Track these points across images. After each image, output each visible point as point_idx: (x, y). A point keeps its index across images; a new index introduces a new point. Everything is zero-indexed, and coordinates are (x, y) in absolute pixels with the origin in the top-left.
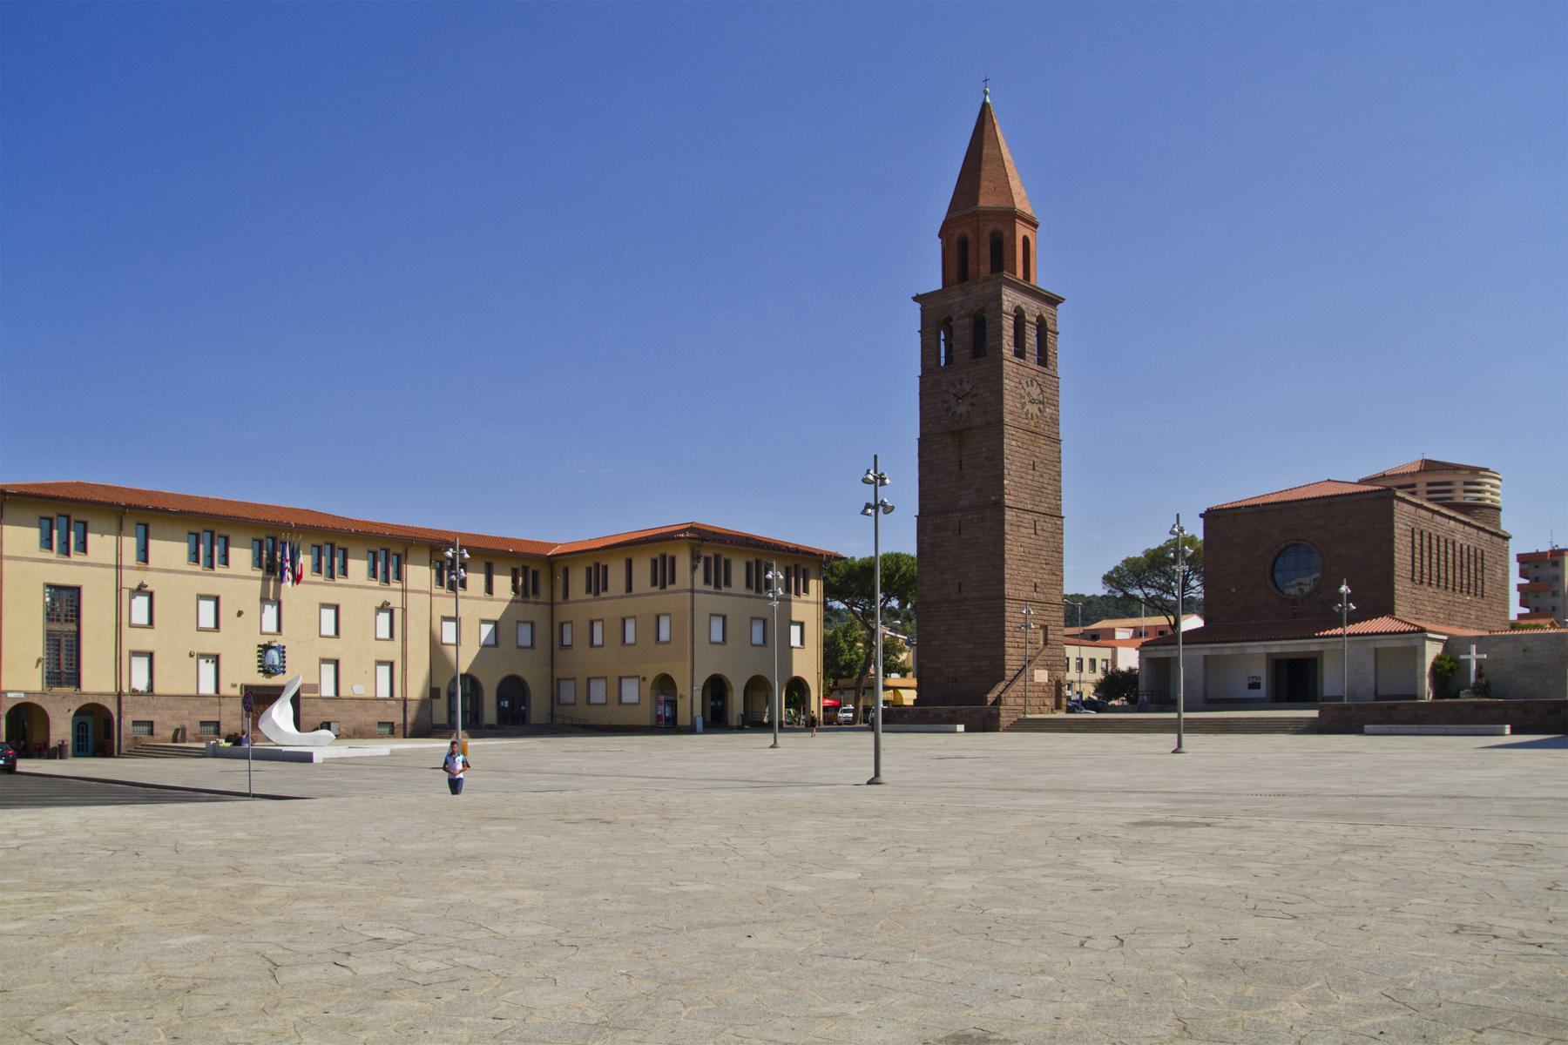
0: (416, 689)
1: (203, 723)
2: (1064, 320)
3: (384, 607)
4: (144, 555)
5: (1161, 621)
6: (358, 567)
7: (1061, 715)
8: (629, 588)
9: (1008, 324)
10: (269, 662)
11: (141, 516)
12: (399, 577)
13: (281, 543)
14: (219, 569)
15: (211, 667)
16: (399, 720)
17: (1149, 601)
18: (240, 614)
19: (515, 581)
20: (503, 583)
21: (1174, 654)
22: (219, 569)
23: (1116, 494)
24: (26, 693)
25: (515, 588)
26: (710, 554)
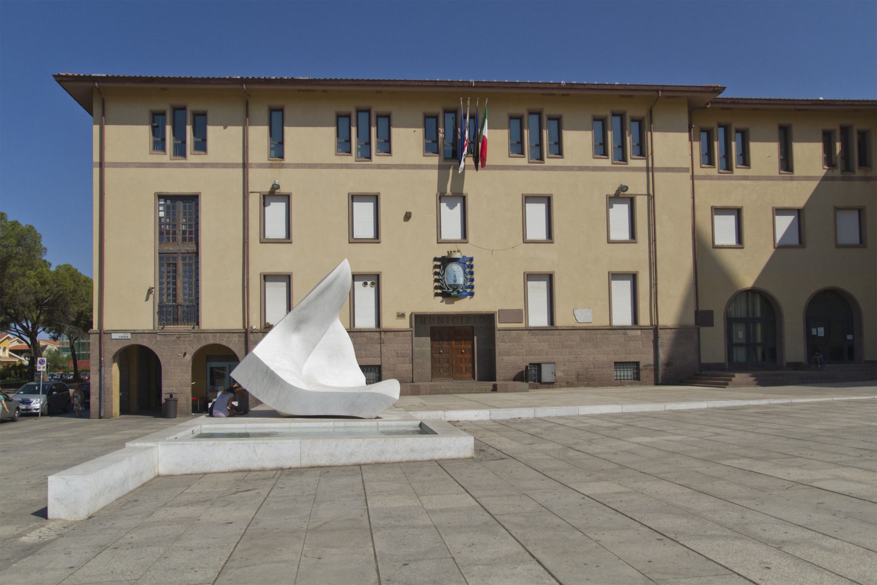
0: (669, 314)
3: (620, 196)
4: (278, 148)
6: (578, 142)
10: (449, 281)
11: (272, 101)
12: (642, 150)
14: (738, 171)
15: (370, 291)
16: (646, 358)
18: (408, 217)
19: (828, 150)
20: (809, 155)
22: (738, 171)
24: (134, 333)
25: (829, 160)
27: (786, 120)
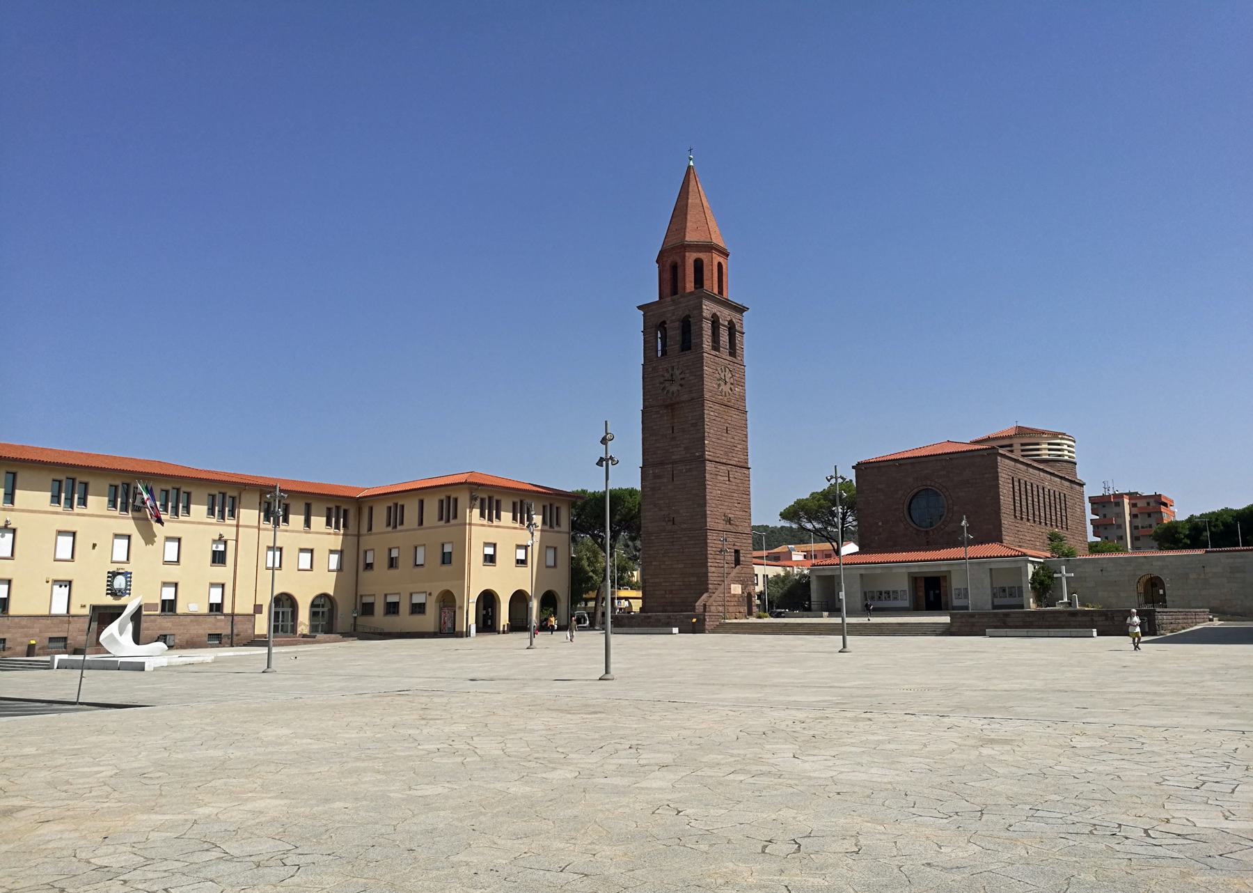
1: (51, 639)
2: (747, 323)
5: (827, 546)
7: (753, 620)
8: (421, 523)
9: (707, 326)
10: (480, 532)
12: (232, 514)
13: (146, 492)
17: (816, 531)
21: (837, 573)
23: (790, 447)
26: (485, 496)
27: (310, 501)
